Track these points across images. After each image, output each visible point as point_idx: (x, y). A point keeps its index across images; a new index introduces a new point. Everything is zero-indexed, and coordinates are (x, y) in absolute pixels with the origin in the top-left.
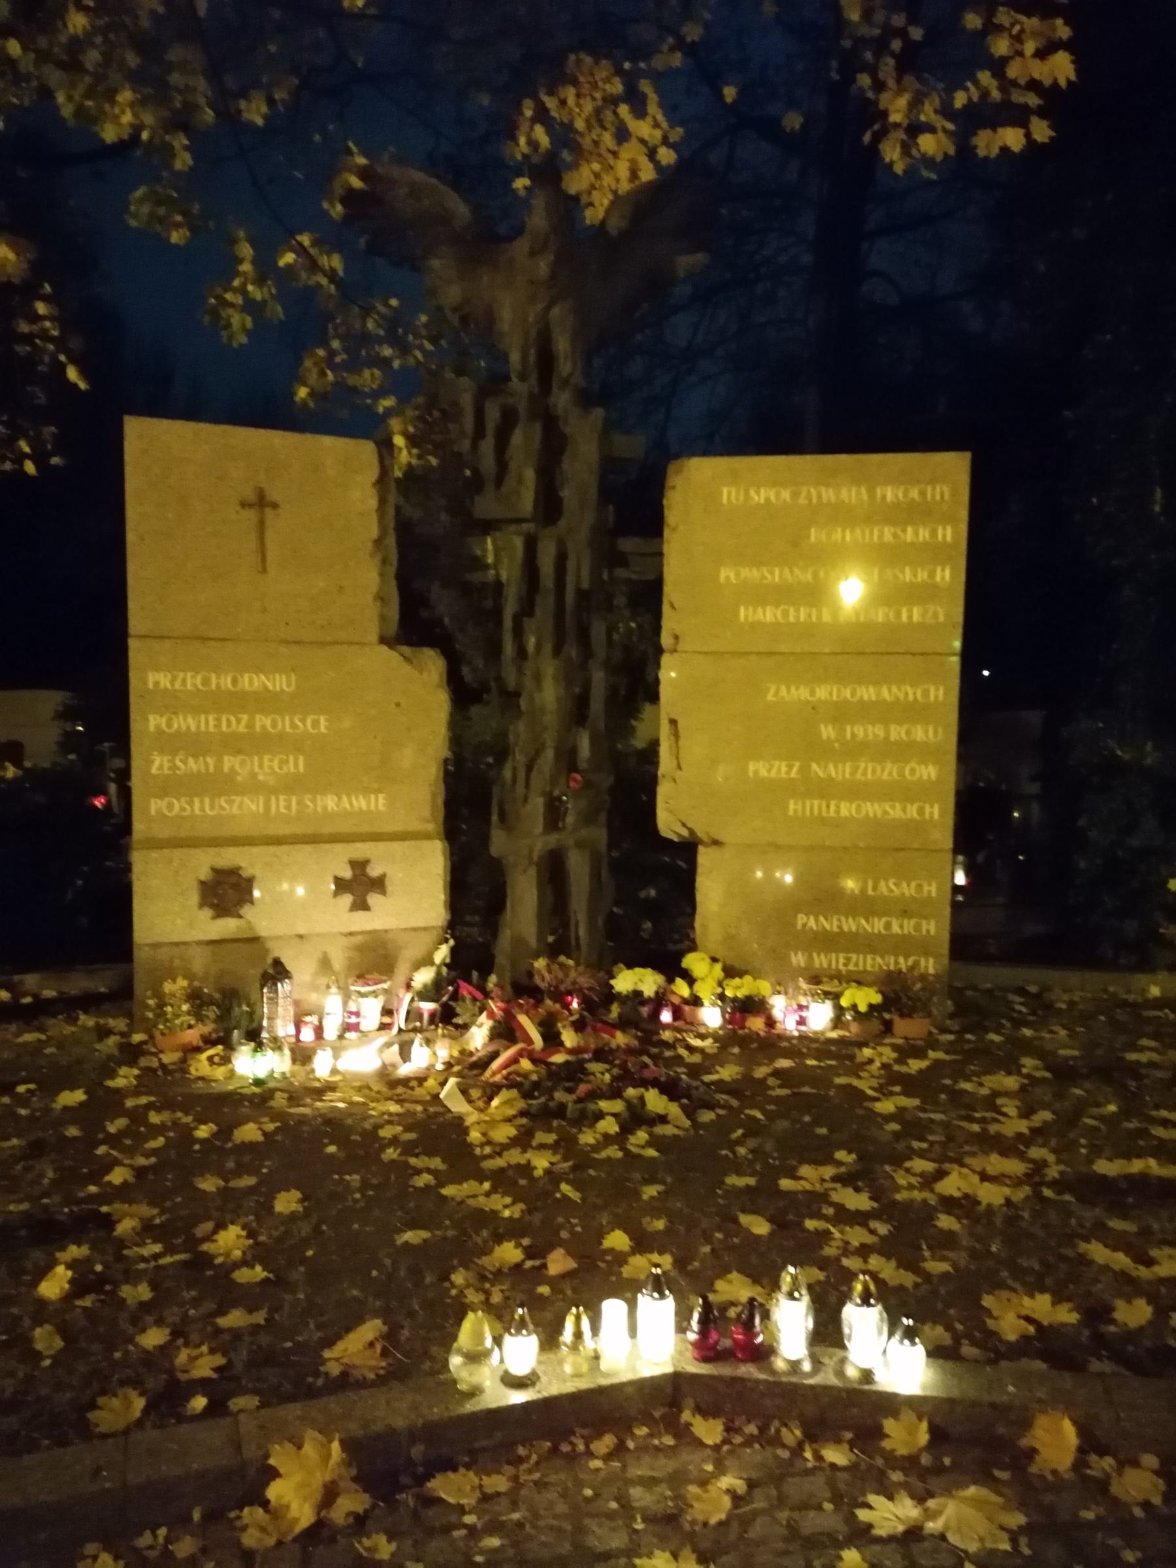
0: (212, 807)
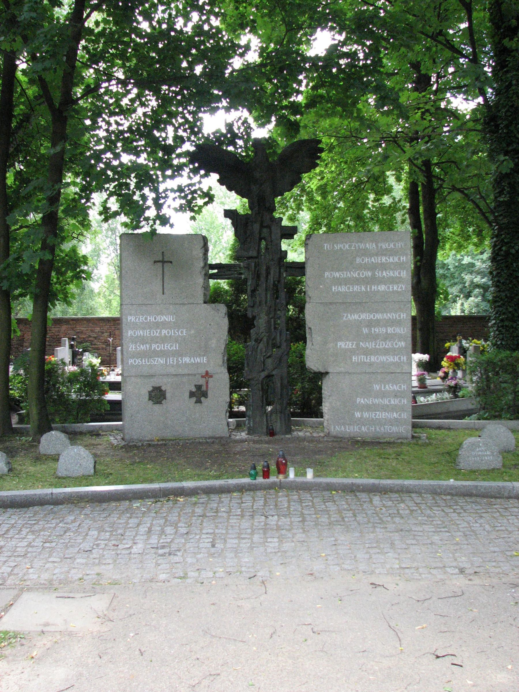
0: (148, 362)
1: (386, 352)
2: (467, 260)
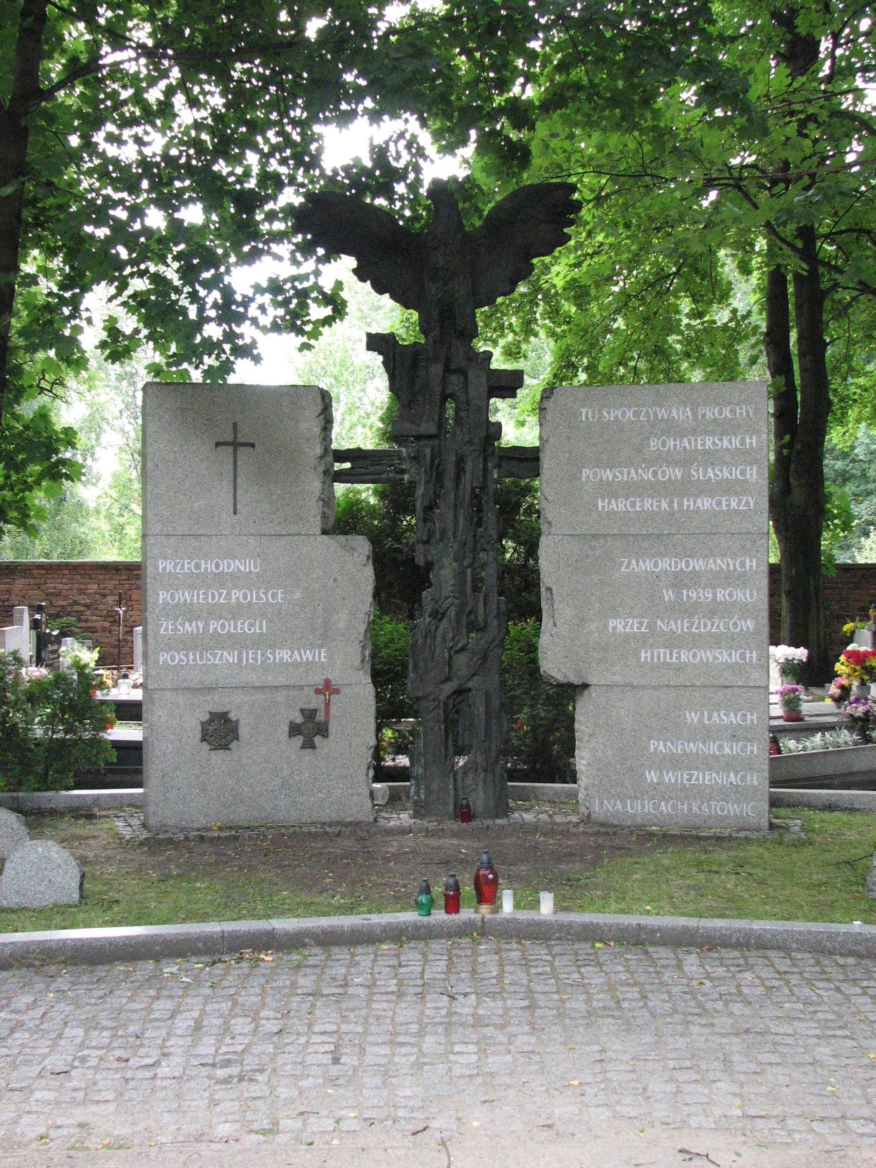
0: (201, 658)
1: (715, 641)
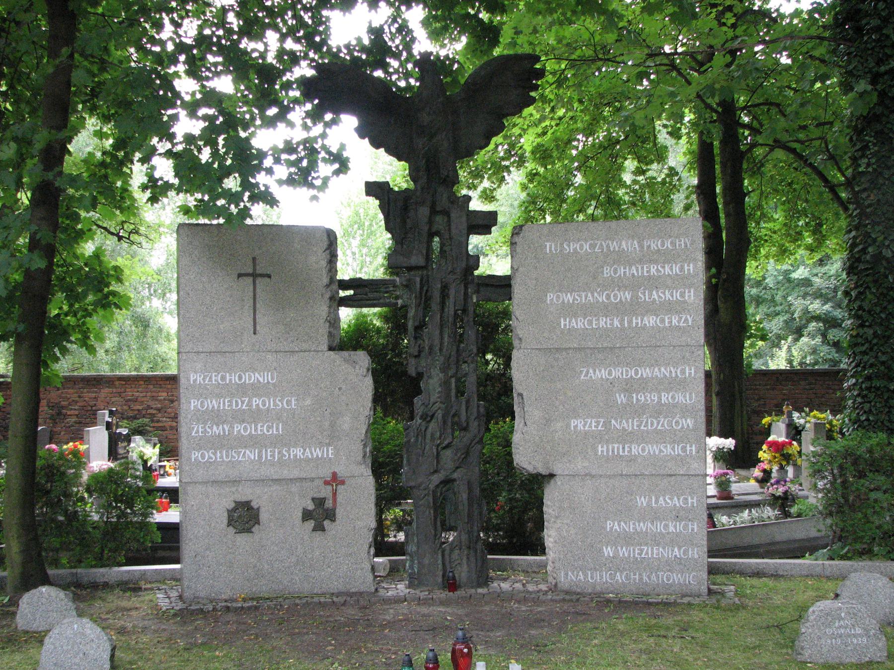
0: (227, 456)
1: (660, 437)
2: (800, 273)
